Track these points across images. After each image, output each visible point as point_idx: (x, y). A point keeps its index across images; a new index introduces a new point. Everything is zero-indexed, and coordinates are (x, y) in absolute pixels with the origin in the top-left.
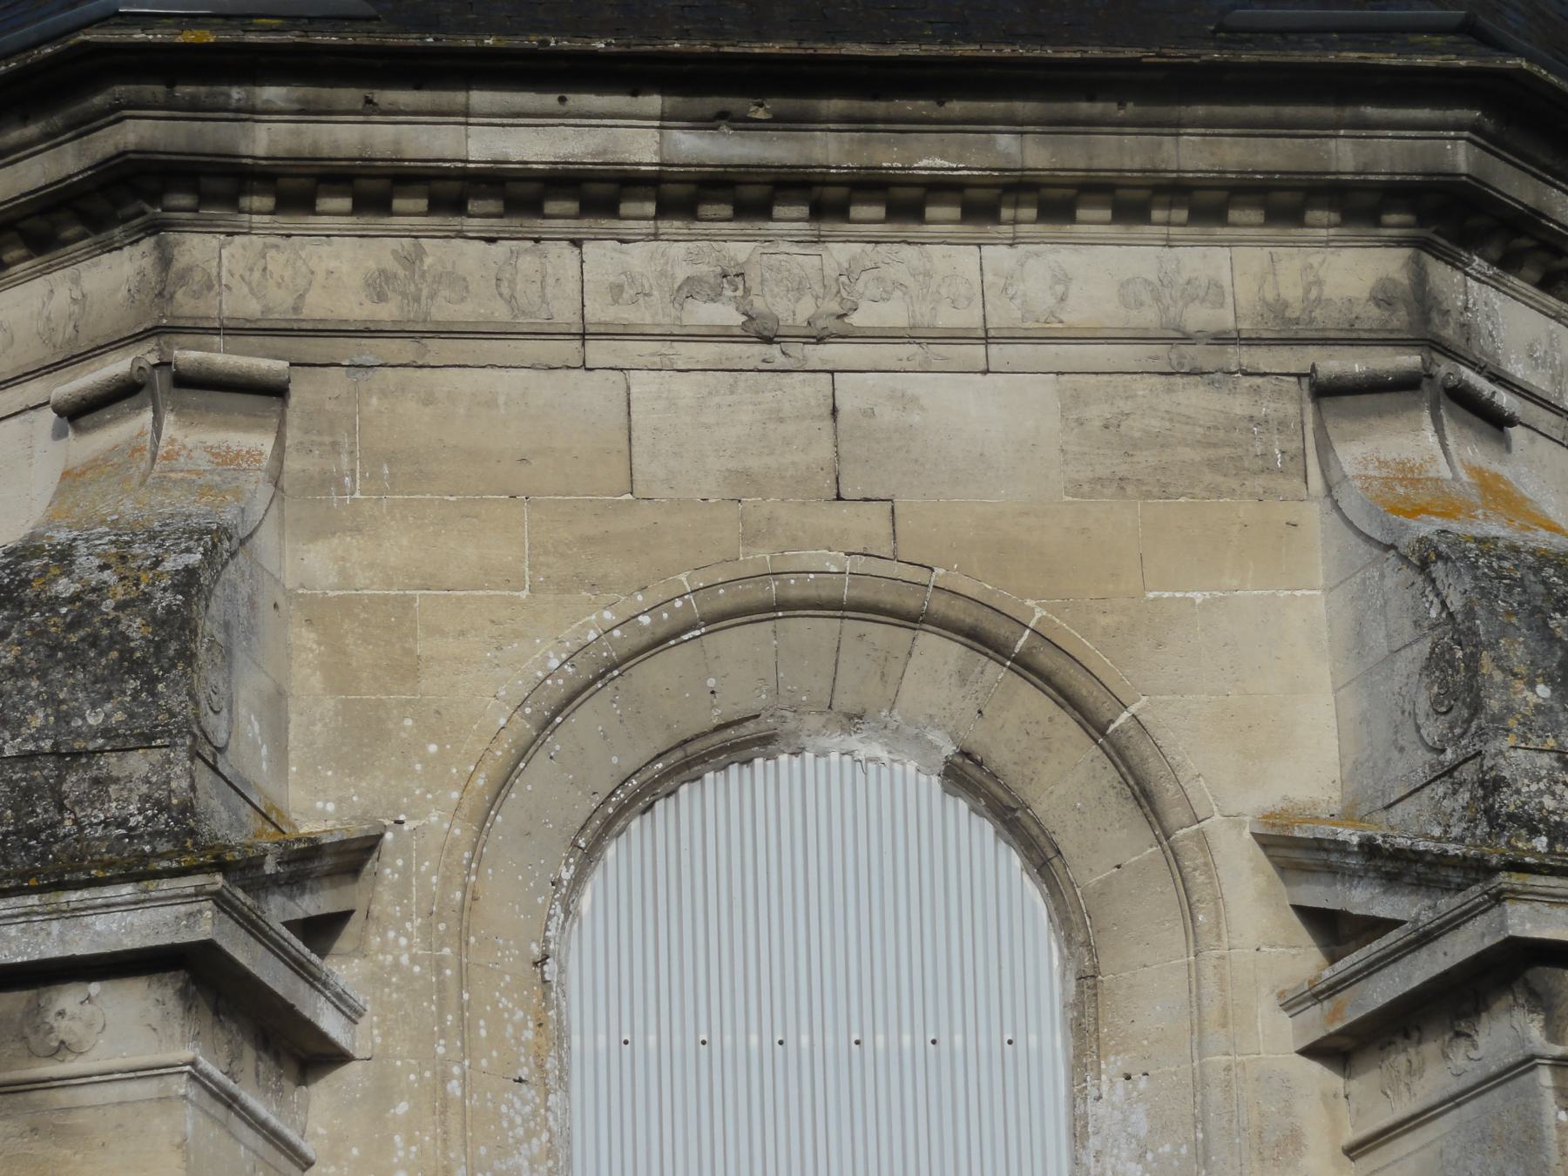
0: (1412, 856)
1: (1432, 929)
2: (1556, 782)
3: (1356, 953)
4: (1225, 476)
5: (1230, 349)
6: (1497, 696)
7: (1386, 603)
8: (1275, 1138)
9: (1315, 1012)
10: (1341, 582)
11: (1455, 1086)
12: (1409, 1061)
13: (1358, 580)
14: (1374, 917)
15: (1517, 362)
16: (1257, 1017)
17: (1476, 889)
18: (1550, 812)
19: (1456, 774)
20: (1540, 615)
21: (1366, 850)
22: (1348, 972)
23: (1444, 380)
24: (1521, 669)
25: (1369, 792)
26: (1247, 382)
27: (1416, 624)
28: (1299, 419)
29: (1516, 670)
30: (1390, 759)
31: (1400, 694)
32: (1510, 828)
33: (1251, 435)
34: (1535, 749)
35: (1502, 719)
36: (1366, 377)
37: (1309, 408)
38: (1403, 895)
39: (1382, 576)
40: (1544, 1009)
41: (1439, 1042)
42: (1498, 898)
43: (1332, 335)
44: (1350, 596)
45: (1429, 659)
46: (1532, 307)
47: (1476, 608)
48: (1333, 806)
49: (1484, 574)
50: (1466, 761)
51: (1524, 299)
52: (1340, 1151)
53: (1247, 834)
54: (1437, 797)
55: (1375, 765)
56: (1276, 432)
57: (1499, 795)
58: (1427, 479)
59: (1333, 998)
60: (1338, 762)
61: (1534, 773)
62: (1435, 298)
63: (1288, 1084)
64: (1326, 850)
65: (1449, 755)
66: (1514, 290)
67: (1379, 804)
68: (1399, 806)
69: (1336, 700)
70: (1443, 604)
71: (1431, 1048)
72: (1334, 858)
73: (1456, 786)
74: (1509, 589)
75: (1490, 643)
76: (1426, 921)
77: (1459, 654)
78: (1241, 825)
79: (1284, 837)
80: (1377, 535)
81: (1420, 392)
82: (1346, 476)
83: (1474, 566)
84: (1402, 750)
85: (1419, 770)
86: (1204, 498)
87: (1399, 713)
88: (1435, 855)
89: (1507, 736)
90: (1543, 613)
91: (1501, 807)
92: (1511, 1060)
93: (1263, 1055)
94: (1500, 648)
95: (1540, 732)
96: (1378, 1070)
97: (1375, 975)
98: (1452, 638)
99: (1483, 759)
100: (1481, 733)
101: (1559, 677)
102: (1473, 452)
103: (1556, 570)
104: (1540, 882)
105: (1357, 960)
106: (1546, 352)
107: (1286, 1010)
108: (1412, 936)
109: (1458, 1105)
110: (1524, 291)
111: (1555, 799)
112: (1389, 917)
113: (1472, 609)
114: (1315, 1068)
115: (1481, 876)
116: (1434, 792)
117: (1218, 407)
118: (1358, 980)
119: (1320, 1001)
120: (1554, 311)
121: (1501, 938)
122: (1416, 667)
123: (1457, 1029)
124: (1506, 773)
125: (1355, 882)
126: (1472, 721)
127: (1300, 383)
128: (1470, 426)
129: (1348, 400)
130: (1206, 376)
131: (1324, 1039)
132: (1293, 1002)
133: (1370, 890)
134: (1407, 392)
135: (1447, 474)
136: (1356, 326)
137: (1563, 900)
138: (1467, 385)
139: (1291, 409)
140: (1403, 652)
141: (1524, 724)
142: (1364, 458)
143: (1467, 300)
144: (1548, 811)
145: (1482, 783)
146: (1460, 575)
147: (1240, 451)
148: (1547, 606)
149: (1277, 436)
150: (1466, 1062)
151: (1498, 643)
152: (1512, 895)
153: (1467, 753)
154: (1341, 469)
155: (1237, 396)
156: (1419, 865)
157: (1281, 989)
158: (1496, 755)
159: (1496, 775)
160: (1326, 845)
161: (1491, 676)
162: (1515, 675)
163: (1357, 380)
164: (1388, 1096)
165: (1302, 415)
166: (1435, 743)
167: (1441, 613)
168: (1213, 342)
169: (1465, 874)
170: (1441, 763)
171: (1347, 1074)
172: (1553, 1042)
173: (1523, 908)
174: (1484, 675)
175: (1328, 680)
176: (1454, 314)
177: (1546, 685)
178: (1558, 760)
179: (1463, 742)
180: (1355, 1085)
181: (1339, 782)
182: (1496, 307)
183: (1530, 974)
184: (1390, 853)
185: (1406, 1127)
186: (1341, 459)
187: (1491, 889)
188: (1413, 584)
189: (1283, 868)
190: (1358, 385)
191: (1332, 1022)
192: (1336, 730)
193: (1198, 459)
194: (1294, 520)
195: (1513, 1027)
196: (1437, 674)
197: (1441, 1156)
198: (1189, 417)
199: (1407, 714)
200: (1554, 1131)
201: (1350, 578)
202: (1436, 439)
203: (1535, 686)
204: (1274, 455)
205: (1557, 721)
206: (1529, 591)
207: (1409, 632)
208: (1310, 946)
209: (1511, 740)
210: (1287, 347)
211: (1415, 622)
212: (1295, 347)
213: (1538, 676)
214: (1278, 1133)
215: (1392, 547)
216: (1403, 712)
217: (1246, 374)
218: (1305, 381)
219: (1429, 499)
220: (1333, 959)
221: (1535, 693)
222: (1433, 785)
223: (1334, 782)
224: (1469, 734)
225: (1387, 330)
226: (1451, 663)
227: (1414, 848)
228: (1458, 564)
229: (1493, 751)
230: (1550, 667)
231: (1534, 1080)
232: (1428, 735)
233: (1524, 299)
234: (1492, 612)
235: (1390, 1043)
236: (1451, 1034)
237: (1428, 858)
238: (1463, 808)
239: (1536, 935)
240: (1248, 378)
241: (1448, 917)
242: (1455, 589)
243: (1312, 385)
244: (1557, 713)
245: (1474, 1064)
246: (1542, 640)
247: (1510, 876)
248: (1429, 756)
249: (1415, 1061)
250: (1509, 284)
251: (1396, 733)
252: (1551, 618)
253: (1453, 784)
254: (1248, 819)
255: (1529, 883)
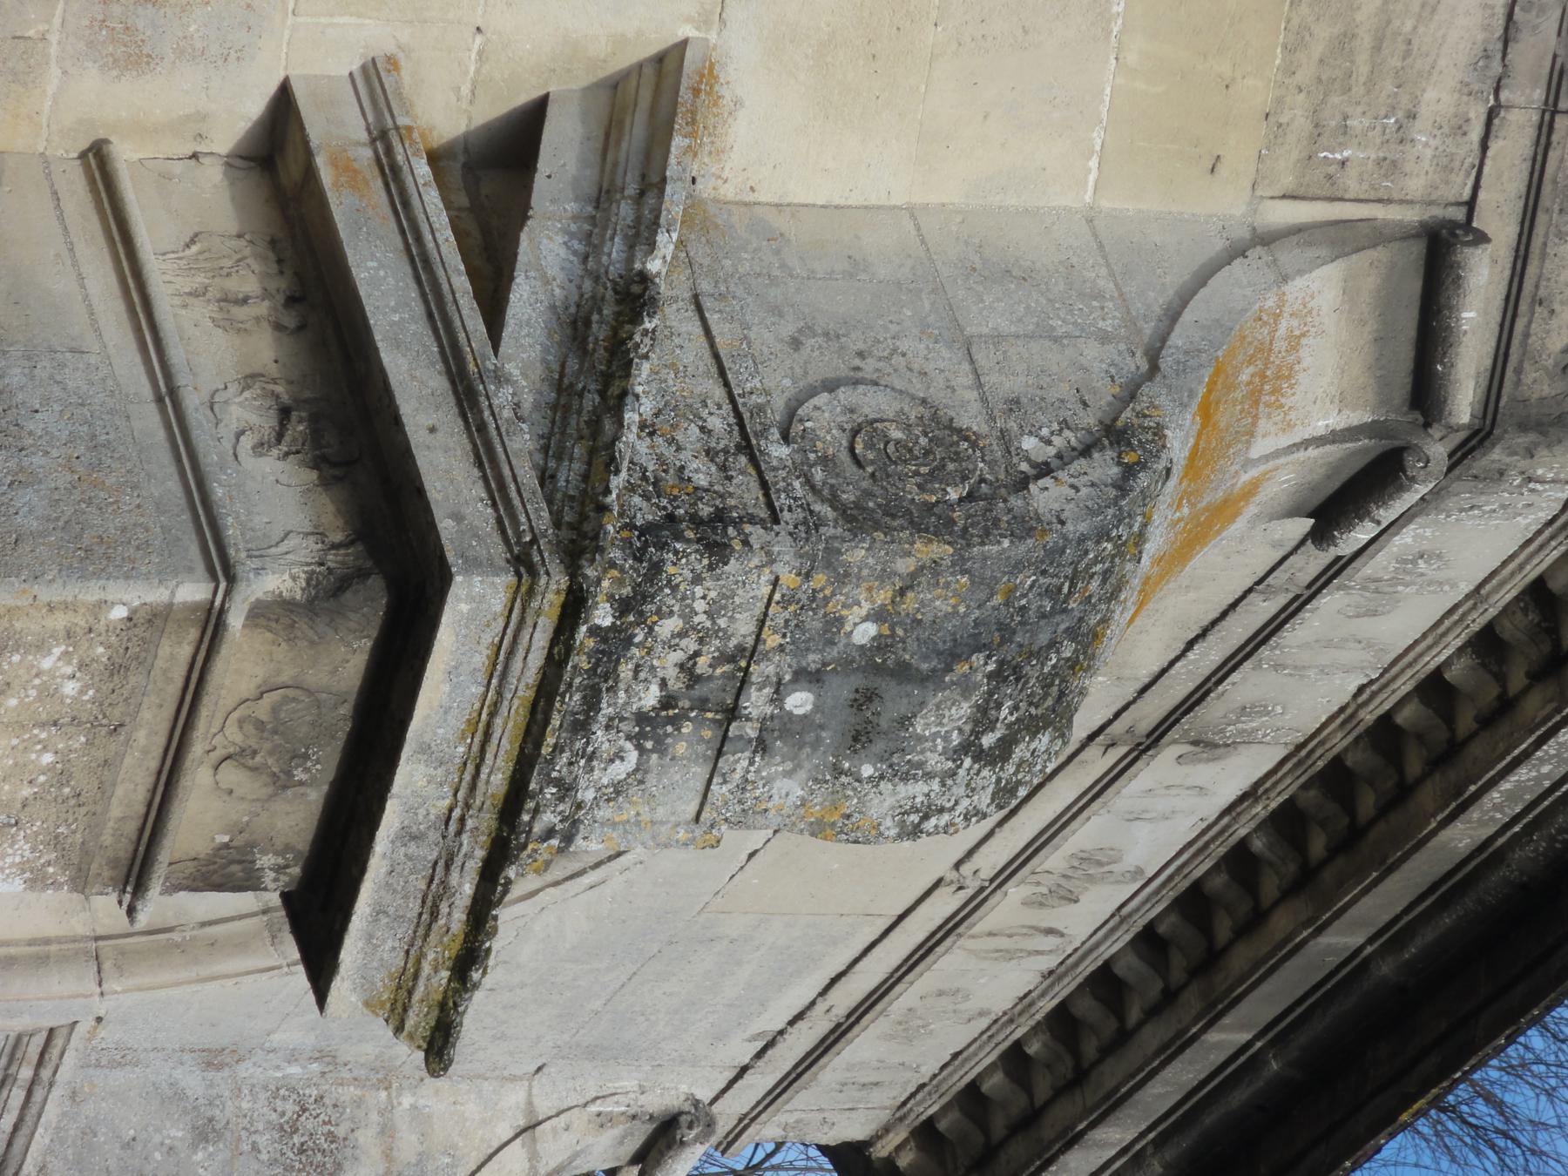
0: (614, 390)
1: (481, 412)
2: (701, 641)
3: (452, 239)
4: (1321, 61)
5: (1539, 94)
6: (871, 561)
7: (1056, 340)
8: (140, 28)
9: (355, 128)
10: (1101, 246)
11: (192, 401)
12: (245, 301)
13: (1101, 283)
14: (512, 279)
15: (1415, 537)
16: (360, 16)
17: (543, 520)
18: (651, 629)
19: (743, 460)
20: (997, 640)
21: (636, 289)
22: (421, 217)
23: (1416, 449)
24: (910, 603)
25: (727, 263)
26: (1477, 114)
27: (1014, 404)
28: (1396, 196)
29: (910, 595)
30: (781, 315)
31: (895, 351)
32: (636, 570)
33: (1383, 113)
34: (766, 614)
35: (828, 565)
36: (1449, 327)
37: (1411, 216)
38: (546, 350)
39: (1105, 338)
40: (311, 602)
41: (274, 370)
42: (522, 563)
43: (1532, 270)
44: (1074, 260)
45: (950, 426)
46: (1504, 564)
47: (1030, 542)
48: (711, 185)
49: (1086, 552)
50: (764, 485)
51: (1522, 556)
52: (101, 134)
53: (687, 31)
54: (704, 414)
55: (774, 281)
56: (1381, 155)
57: (697, 551)
58: (1256, 418)
59: (376, 172)
60: (786, 201)
61: (724, 607)
62: (1560, 442)
63: (233, 55)
64: (642, 193)
65: (779, 452)
66: (1541, 547)
67: (705, 286)
68: (697, 330)
69: (894, 207)
70: (1044, 470)
71: (264, 350)
72: (625, 210)
73: (722, 457)
74: (1052, 593)
75: (964, 560)
76: (495, 402)
77: (953, 495)
78: (704, 22)
79: (674, 114)
80: (1177, 339)
81: (1405, 409)
82: (1285, 279)
83: (1102, 535)
84: (796, 344)
85: (756, 382)
86: (1288, 21)
87: (861, 346)
88: (613, 443)
89: (799, 574)
90: (1000, 645)
91: (676, 552)
92: (231, 532)
93: (290, 20)
94: (953, 574)
95: (793, 623)
96: (234, 230)
97: (408, 269)
98: (982, 480)
99: (762, 522)
100: (812, 524)
101: (885, 661)
102: (1284, 482)
103: (1068, 659)
104: (541, 639)
105: (440, 240)
106: (1422, 575)
107: (364, 68)
108: (471, 367)
109: (159, 400)
110: (1535, 561)
111: (673, 636)
112: (510, 312)
113: (1030, 531)
114: (254, 106)
115: (565, 534)
116: (714, 409)
117: (1442, 62)
118: (403, 232)
119: (373, 141)
120: (1488, 596)
121: (450, 557)
122: (937, 394)
123: (294, 415)
124: (733, 566)
125: (576, 245)
126: (834, 508)
127: (1458, 204)
128: (1329, 477)
129: (1415, 286)
130: (1500, 46)
131: (306, 142)
132: (379, 91)
133: (561, 277)
134: (1409, 387)
135: (1255, 453)
136: (1538, 309)
137: (499, 667)
138: (1401, 489)
139: (1415, 185)
140: (966, 366)
141: (813, 599)
142: (1310, 312)
143: (1542, 482)
144: (655, 623)
145: (720, 517)
146: (1092, 512)
147: (1358, 91)
148: (1010, 652)
149: (1373, 156)
150: (234, 426)
151: (964, 572)
152: (523, 589)
153: (778, 491)
154: (1301, 272)
155: (1456, 96)
156: (597, 399)
157: (403, 63)
158: (769, 554)
159: (733, 550)
160: (651, 200)
161: (908, 554)
162: (902, 592)
163: (1446, 312)
164: (188, 246)
165: (1402, 202)
166: (801, 421)
167: (1028, 460)
168: (1558, 67)
169: (572, 498)
170: (763, 433)
171: (238, 163)
172: (251, 610)
173: (498, 603)
174: (912, 543)
175: (933, 199)
176: (1523, 464)
177: (874, 639)
178: (741, 649)
179: (797, 484)
180: (213, 174)
181: (751, 198)
182: (1519, 518)
183: (376, 583)
184: (623, 342)
185: (130, 281)
186: (1317, 273)
187: (540, 552)
188: (1085, 404)
189: (615, 87)
190: (1439, 311)
191: (334, 163)
192: (842, 202)
193: (1359, 17)
194: (1222, 170)
195: (286, 535)
196: (923, 441)
197: (72, 351)
198: (1434, 10)
199: (857, 362)
200: (96, 597)
201: (1108, 265)
202: (1321, 432)
203: (875, 621)
204: (1342, 146)
205: (808, 649)
206: (1042, 623)
207: (1005, 384)
208: (470, 119)
209: (789, 579)
210: (1523, 190)
211: (1017, 401)
212: (1521, 203)
213: (892, 629)
214: (148, 33)
215: (1154, 368)
216: (861, 354)
217: (1492, 115)
218: (1459, 214)
219: (1222, 425)
220: (434, 158)
221: (866, 619)
222: (727, 407)
223: (752, 189)
224: (810, 498)
225: (1521, 362)
226: (937, 474)
227: (629, 399)
228: (1111, 511)
229: (776, 549)
230: (904, 650)
231: (190, 570)
232: (817, 408)
233: (1522, 556)
234: (1017, 567)
235: (280, 261)
236: (285, 398)
237: (608, 426)
238: (682, 468)
239: (447, 619)
240: (1483, 118)
241: (499, 449)
242: (1069, 501)
243: (1452, 225)
244: (822, 651)
245: (227, 445)
246: (955, 640)
247: (558, 592)
248: (779, 403)
249: (240, 313)
250: (1553, 543)
251: (826, 334)
252: (989, 657)
253: (726, 451)
254: (713, 37)
255: (541, 621)
